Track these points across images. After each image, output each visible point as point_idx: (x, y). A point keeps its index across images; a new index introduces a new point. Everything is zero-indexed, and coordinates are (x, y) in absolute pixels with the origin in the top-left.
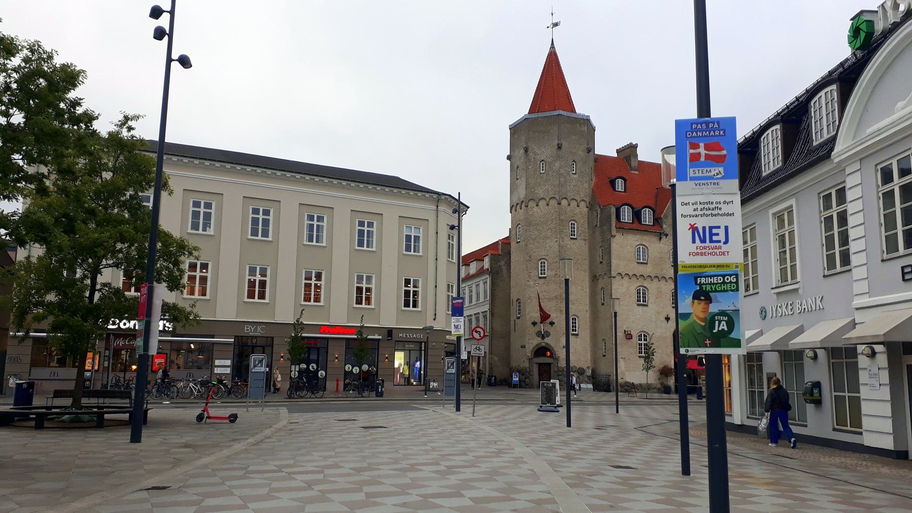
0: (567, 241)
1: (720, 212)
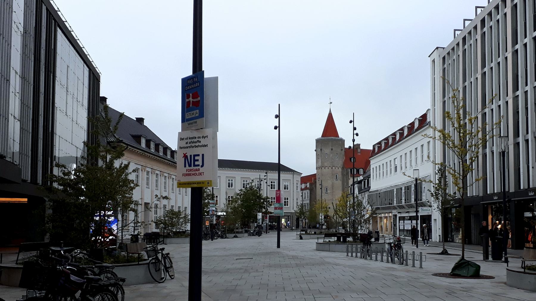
0: (335, 180)
1: (200, 144)
